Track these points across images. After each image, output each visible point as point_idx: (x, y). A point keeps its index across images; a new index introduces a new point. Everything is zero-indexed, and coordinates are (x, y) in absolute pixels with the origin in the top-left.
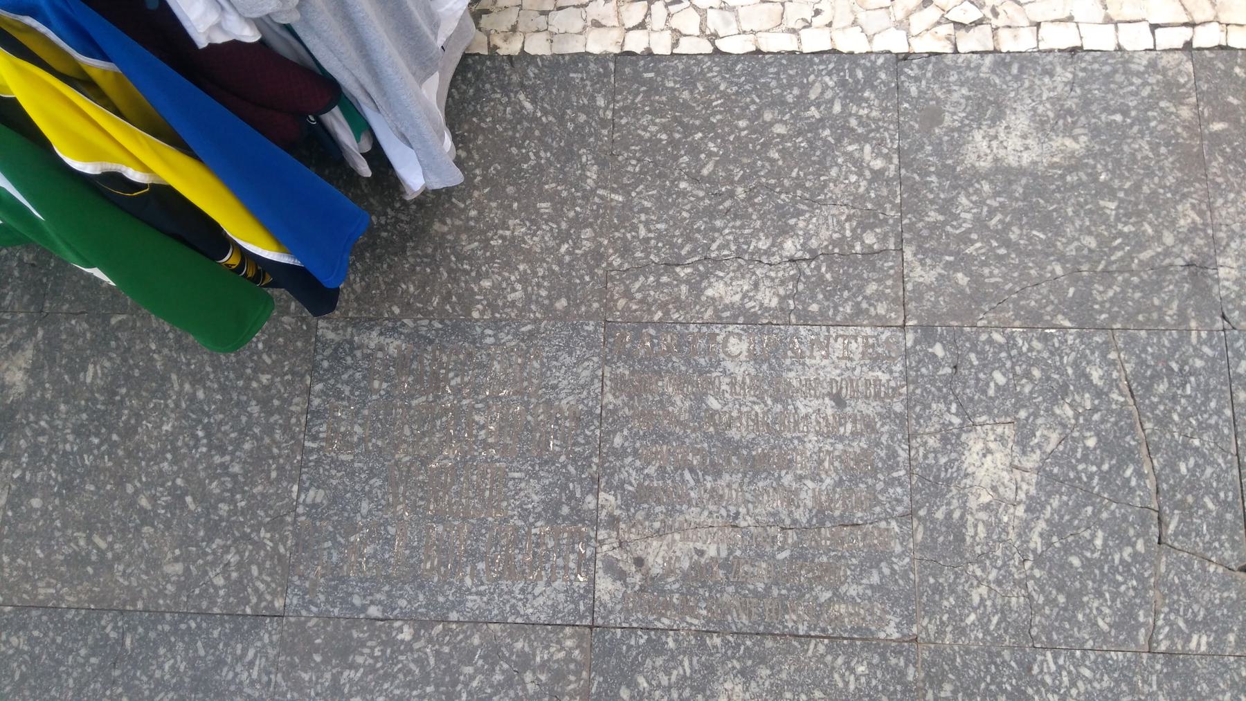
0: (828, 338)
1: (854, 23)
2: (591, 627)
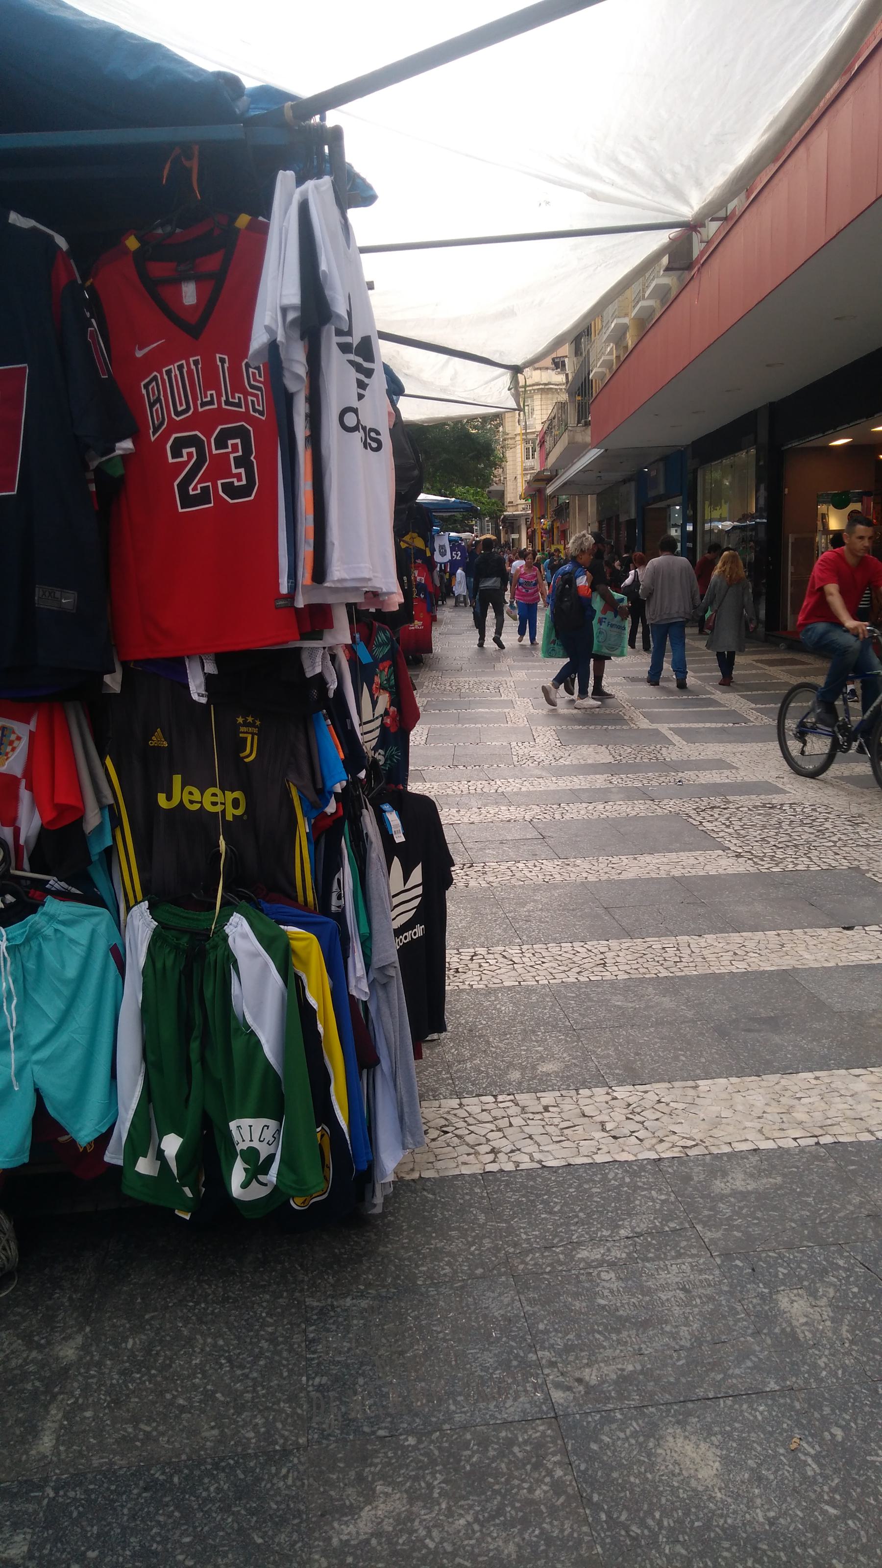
1: (623, 1151)
2: (556, 1418)
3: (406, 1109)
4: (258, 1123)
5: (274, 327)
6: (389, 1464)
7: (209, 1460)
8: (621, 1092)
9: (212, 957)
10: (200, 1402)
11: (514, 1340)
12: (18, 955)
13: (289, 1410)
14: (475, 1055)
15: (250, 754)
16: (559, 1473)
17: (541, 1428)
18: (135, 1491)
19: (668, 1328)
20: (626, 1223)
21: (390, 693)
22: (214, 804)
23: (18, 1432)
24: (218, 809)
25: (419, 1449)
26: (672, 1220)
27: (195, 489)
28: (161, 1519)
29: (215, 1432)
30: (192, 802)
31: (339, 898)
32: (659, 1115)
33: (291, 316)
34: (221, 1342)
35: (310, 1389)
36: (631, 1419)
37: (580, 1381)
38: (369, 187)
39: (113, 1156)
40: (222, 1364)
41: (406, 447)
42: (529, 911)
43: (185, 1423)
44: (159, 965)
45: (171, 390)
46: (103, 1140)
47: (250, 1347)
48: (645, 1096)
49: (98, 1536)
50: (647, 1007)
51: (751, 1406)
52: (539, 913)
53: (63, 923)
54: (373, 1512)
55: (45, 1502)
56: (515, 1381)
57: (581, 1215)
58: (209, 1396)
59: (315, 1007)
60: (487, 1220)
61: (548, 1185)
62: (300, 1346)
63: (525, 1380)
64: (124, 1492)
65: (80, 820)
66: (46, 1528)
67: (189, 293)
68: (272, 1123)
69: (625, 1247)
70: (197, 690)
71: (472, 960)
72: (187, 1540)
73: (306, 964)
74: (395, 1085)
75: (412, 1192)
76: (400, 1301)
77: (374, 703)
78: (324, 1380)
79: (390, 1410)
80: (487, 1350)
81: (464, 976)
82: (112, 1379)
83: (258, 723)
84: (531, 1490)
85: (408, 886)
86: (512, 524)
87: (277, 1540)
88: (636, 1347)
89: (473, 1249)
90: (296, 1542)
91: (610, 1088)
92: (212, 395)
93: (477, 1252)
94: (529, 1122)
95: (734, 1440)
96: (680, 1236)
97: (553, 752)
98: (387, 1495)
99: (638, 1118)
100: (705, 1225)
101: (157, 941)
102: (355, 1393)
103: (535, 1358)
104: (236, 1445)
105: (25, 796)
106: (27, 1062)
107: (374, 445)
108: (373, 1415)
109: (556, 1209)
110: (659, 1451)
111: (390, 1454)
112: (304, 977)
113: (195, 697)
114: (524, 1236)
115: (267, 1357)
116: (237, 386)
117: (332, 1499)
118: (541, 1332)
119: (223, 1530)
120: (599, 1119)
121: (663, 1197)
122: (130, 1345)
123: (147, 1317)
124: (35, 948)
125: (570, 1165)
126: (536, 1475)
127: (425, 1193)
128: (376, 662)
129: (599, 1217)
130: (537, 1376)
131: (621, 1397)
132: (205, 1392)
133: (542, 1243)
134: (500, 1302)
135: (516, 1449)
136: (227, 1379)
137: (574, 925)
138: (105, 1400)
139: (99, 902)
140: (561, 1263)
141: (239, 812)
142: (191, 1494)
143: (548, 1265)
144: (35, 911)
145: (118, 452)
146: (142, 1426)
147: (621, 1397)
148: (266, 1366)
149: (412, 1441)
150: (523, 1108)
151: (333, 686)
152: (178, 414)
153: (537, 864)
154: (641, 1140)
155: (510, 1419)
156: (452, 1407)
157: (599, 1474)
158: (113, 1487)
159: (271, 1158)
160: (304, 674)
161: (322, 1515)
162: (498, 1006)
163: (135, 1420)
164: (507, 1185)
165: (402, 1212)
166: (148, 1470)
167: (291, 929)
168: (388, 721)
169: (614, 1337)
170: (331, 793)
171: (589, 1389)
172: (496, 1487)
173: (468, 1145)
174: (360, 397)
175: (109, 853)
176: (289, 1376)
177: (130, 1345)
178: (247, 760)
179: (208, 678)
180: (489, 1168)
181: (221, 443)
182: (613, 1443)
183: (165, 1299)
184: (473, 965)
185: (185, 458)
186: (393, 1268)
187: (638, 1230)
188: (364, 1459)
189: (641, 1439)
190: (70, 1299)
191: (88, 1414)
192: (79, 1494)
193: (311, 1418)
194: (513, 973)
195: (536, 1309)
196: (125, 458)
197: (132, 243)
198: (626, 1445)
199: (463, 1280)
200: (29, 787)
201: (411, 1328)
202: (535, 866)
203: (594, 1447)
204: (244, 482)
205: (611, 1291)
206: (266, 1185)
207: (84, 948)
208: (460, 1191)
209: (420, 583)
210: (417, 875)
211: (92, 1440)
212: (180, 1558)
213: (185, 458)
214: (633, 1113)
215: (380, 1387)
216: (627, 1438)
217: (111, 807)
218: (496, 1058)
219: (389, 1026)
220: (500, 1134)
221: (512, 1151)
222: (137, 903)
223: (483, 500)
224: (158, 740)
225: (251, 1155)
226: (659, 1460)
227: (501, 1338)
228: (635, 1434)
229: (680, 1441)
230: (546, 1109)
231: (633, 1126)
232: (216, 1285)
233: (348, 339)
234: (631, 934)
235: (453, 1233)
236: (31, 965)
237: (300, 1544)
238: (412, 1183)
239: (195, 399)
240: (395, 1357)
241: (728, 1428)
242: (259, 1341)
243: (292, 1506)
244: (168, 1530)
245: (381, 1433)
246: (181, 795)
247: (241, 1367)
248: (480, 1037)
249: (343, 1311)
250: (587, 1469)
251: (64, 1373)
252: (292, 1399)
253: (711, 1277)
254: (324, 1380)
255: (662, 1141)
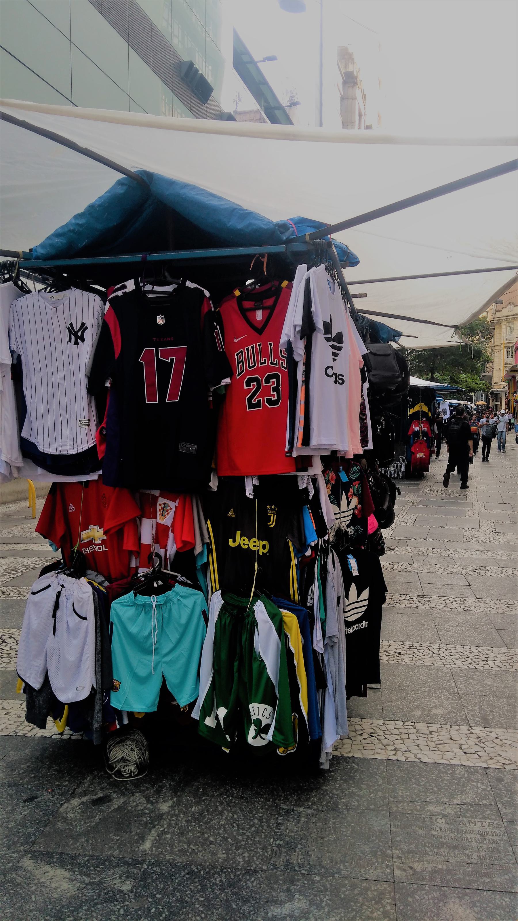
0: (475, 822)
1: (468, 760)
2: (394, 883)
3: (339, 714)
4: (263, 706)
5: (289, 334)
6: (304, 886)
7: (219, 867)
8: (477, 730)
9: (246, 621)
10: (220, 841)
11: (382, 842)
12: (160, 609)
13: (261, 853)
14: (398, 699)
15: (272, 524)
16: (388, 907)
17: (385, 886)
18: (183, 874)
19: (467, 852)
20: (459, 797)
21: (359, 498)
22: (254, 546)
23: (136, 838)
24: (256, 549)
25: (320, 883)
26: (485, 800)
27: (255, 401)
28: (192, 888)
29: (225, 856)
30: (244, 544)
31: (311, 599)
32: (494, 745)
33: (298, 329)
34: (235, 816)
35: (274, 845)
36: (433, 891)
37: (411, 868)
38: (356, 258)
39: (195, 715)
40: (234, 827)
41: (395, 365)
42: (450, 626)
43: (211, 849)
44: (223, 623)
45: (247, 357)
46: (192, 705)
47: (249, 821)
48: (490, 734)
49: (163, 889)
50: (506, 687)
51: (501, 898)
52: (456, 628)
53: (182, 597)
54: (291, 906)
55: (142, 870)
56: (377, 862)
57: (435, 789)
58: (225, 839)
59: (293, 651)
60: (383, 783)
61: (421, 771)
62: (273, 825)
63: (383, 862)
64: (178, 873)
65: (193, 549)
66: (141, 881)
67: (259, 315)
68: (270, 709)
69: (455, 808)
70: (249, 492)
71: (410, 649)
72: (202, 899)
73: (290, 629)
74: (335, 698)
75: (347, 763)
76: (328, 813)
77: (349, 503)
78: (281, 843)
80: (367, 844)
81: (403, 657)
82: (182, 823)
83: (277, 509)
84: (372, 912)
85: (359, 599)
86: (496, 396)
87: (243, 908)
88: (446, 858)
89: (372, 795)
90: (251, 911)
91: (471, 727)
92: (265, 360)
93: (373, 797)
94: (419, 738)
95: (486, 911)
96: (488, 808)
97: (489, 536)
98: (299, 899)
99: (482, 745)
100: (503, 804)
101: (224, 609)
102: (295, 852)
103: (390, 852)
104: (233, 863)
105: (171, 535)
106: (159, 662)
107: (341, 381)
109: (422, 784)
110: (444, 908)
111: (305, 882)
112: (289, 636)
113: (248, 495)
114: (401, 794)
115: (256, 827)
116: (276, 356)
117: (272, 896)
118: (397, 841)
119: (219, 898)
120: (460, 742)
121: (484, 787)
122: (193, 810)
123: (203, 798)
124: (168, 607)
125: (436, 763)
126: (376, 906)
127: (354, 764)
128: (351, 482)
129: (444, 792)
130: (389, 862)
131: (431, 879)
132: (224, 837)
133: (410, 799)
134: (379, 823)
135: (369, 893)
136: (235, 833)
137: (474, 637)
138: (177, 832)
139: (199, 588)
140: (417, 810)
141: (265, 551)
142: (208, 880)
143: (410, 810)
144: (170, 590)
145: (222, 384)
146: (192, 846)
147: (431, 879)
148: (254, 831)
149: (318, 878)
150: (418, 730)
151: (312, 494)
152: (250, 367)
153: (462, 600)
154: (480, 757)
155: (370, 879)
156: (342, 867)
157: (409, 912)
158: (173, 870)
159: (268, 726)
160: (298, 487)
161: (267, 902)
162: (418, 675)
163: (189, 843)
164: (398, 768)
165: (339, 771)
166: (191, 866)
167: (285, 612)
168: (357, 512)
169: (436, 851)
170: (309, 545)
171: (415, 872)
172: (354, 908)
173: (382, 744)
174: (334, 360)
175: (206, 566)
176: (265, 838)
177: (193, 810)
178: (271, 526)
179: (255, 486)
180: (391, 758)
181: (267, 381)
182: (420, 900)
183: (213, 792)
184: (410, 652)
185: (252, 387)
186: (328, 798)
187: (465, 801)
188: (292, 881)
189: (436, 901)
190: (170, 784)
191: (168, 836)
192: (157, 869)
193: (271, 859)
194: (432, 659)
195: (397, 830)
196: (226, 386)
197: (237, 293)
198: (427, 902)
199: (363, 810)
200: (172, 532)
201: (330, 827)
202: (460, 601)
203: (410, 899)
204: (276, 398)
205: (441, 829)
206: (264, 739)
207: (190, 610)
208: (372, 766)
209: (424, 431)
210: (366, 594)
212: (197, 906)
213: (252, 387)
214: (480, 742)
215: (308, 851)
216: (429, 899)
217: (208, 544)
218: (410, 703)
219: (333, 669)
220: (402, 742)
221: (406, 751)
222: (216, 591)
223: (477, 382)
224: (231, 514)
225: (258, 722)
226: (443, 912)
227: (375, 840)
228: (434, 898)
229: (456, 906)
230: (431, 733)
231: (477, 748)
232: (239, 790)
233: (329, 336)
234: (508, 645)
235: (363, 786)
236: (166, 615)
237: (253, 912)
238: (348, 759)
239: (258, 361)
240: (319, 839)
241: (485, 905)
242: (254, 819)
243: (253, 895)
244: (194, 893)
245: (303, 872)
246: (240, 541)
247: (243, 829)
248: (403, 690)
249: (298, 813)
250: (403, 909)
251: (160, 817)
252: (264, 848)
253: (498, 832)
254: (281, 843)
255: (492, 759)
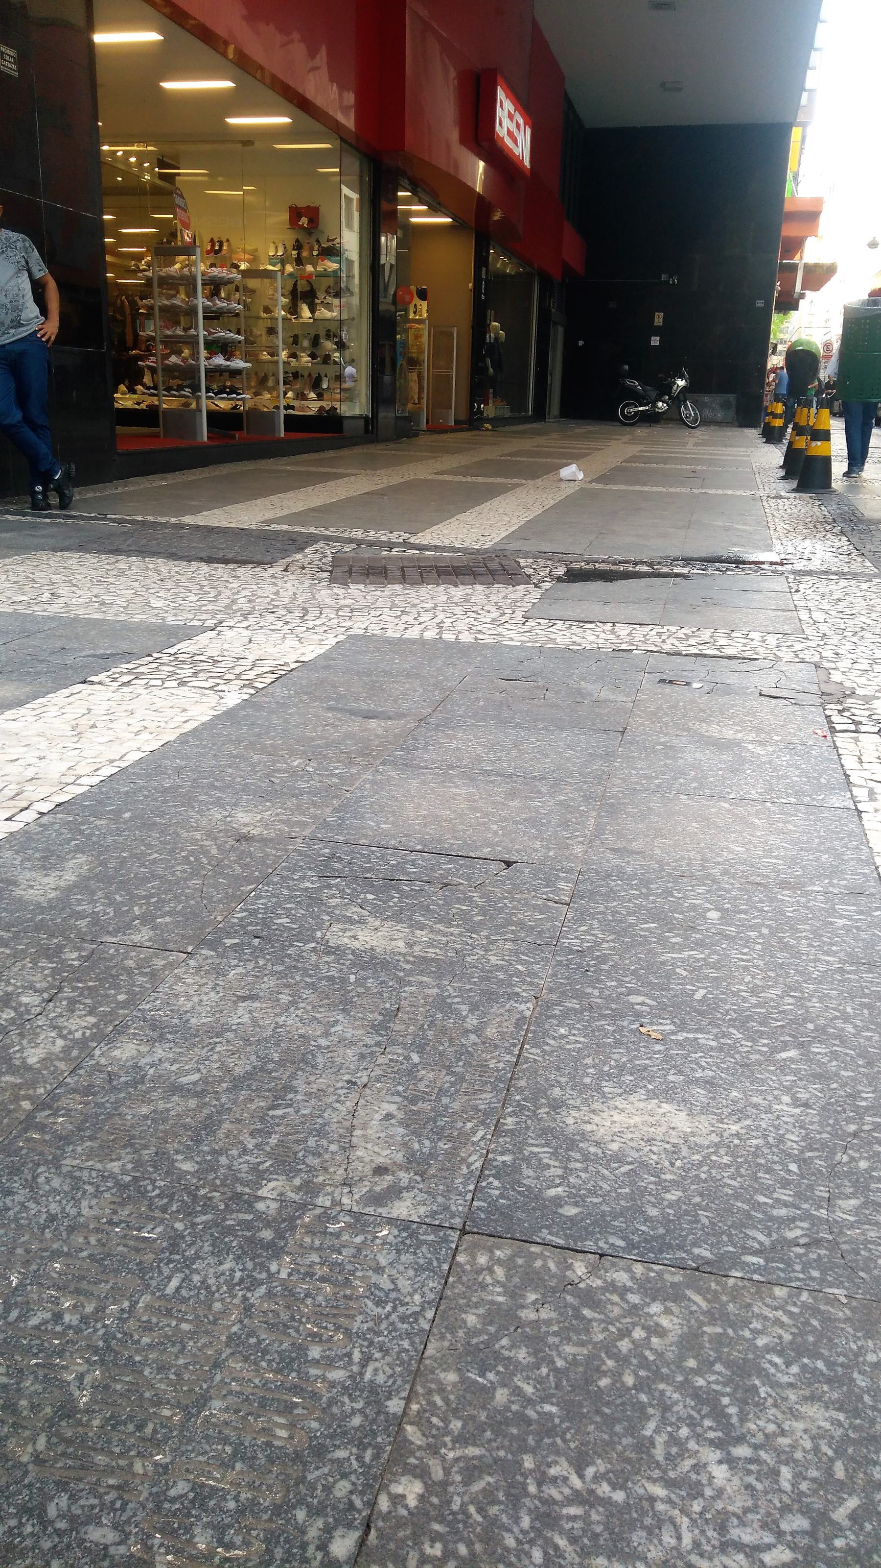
79: (265, 1502)
108: (258, 1546)
211: (554, 1409)
